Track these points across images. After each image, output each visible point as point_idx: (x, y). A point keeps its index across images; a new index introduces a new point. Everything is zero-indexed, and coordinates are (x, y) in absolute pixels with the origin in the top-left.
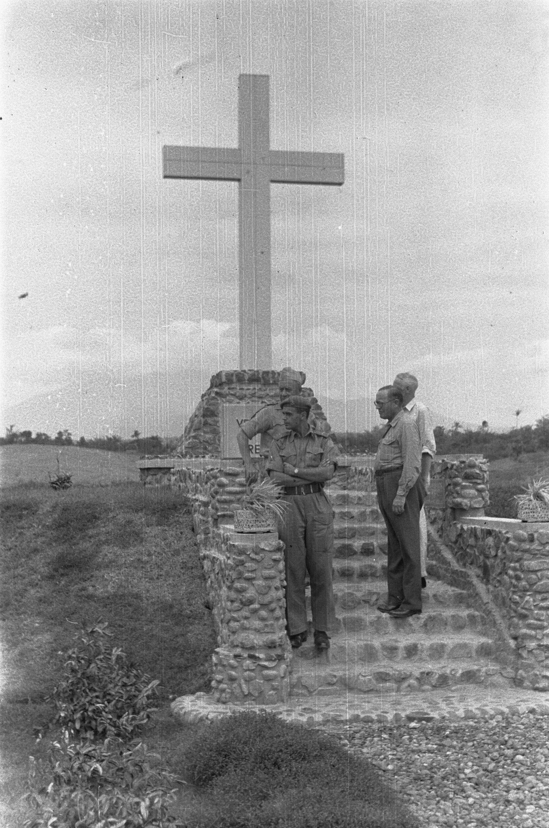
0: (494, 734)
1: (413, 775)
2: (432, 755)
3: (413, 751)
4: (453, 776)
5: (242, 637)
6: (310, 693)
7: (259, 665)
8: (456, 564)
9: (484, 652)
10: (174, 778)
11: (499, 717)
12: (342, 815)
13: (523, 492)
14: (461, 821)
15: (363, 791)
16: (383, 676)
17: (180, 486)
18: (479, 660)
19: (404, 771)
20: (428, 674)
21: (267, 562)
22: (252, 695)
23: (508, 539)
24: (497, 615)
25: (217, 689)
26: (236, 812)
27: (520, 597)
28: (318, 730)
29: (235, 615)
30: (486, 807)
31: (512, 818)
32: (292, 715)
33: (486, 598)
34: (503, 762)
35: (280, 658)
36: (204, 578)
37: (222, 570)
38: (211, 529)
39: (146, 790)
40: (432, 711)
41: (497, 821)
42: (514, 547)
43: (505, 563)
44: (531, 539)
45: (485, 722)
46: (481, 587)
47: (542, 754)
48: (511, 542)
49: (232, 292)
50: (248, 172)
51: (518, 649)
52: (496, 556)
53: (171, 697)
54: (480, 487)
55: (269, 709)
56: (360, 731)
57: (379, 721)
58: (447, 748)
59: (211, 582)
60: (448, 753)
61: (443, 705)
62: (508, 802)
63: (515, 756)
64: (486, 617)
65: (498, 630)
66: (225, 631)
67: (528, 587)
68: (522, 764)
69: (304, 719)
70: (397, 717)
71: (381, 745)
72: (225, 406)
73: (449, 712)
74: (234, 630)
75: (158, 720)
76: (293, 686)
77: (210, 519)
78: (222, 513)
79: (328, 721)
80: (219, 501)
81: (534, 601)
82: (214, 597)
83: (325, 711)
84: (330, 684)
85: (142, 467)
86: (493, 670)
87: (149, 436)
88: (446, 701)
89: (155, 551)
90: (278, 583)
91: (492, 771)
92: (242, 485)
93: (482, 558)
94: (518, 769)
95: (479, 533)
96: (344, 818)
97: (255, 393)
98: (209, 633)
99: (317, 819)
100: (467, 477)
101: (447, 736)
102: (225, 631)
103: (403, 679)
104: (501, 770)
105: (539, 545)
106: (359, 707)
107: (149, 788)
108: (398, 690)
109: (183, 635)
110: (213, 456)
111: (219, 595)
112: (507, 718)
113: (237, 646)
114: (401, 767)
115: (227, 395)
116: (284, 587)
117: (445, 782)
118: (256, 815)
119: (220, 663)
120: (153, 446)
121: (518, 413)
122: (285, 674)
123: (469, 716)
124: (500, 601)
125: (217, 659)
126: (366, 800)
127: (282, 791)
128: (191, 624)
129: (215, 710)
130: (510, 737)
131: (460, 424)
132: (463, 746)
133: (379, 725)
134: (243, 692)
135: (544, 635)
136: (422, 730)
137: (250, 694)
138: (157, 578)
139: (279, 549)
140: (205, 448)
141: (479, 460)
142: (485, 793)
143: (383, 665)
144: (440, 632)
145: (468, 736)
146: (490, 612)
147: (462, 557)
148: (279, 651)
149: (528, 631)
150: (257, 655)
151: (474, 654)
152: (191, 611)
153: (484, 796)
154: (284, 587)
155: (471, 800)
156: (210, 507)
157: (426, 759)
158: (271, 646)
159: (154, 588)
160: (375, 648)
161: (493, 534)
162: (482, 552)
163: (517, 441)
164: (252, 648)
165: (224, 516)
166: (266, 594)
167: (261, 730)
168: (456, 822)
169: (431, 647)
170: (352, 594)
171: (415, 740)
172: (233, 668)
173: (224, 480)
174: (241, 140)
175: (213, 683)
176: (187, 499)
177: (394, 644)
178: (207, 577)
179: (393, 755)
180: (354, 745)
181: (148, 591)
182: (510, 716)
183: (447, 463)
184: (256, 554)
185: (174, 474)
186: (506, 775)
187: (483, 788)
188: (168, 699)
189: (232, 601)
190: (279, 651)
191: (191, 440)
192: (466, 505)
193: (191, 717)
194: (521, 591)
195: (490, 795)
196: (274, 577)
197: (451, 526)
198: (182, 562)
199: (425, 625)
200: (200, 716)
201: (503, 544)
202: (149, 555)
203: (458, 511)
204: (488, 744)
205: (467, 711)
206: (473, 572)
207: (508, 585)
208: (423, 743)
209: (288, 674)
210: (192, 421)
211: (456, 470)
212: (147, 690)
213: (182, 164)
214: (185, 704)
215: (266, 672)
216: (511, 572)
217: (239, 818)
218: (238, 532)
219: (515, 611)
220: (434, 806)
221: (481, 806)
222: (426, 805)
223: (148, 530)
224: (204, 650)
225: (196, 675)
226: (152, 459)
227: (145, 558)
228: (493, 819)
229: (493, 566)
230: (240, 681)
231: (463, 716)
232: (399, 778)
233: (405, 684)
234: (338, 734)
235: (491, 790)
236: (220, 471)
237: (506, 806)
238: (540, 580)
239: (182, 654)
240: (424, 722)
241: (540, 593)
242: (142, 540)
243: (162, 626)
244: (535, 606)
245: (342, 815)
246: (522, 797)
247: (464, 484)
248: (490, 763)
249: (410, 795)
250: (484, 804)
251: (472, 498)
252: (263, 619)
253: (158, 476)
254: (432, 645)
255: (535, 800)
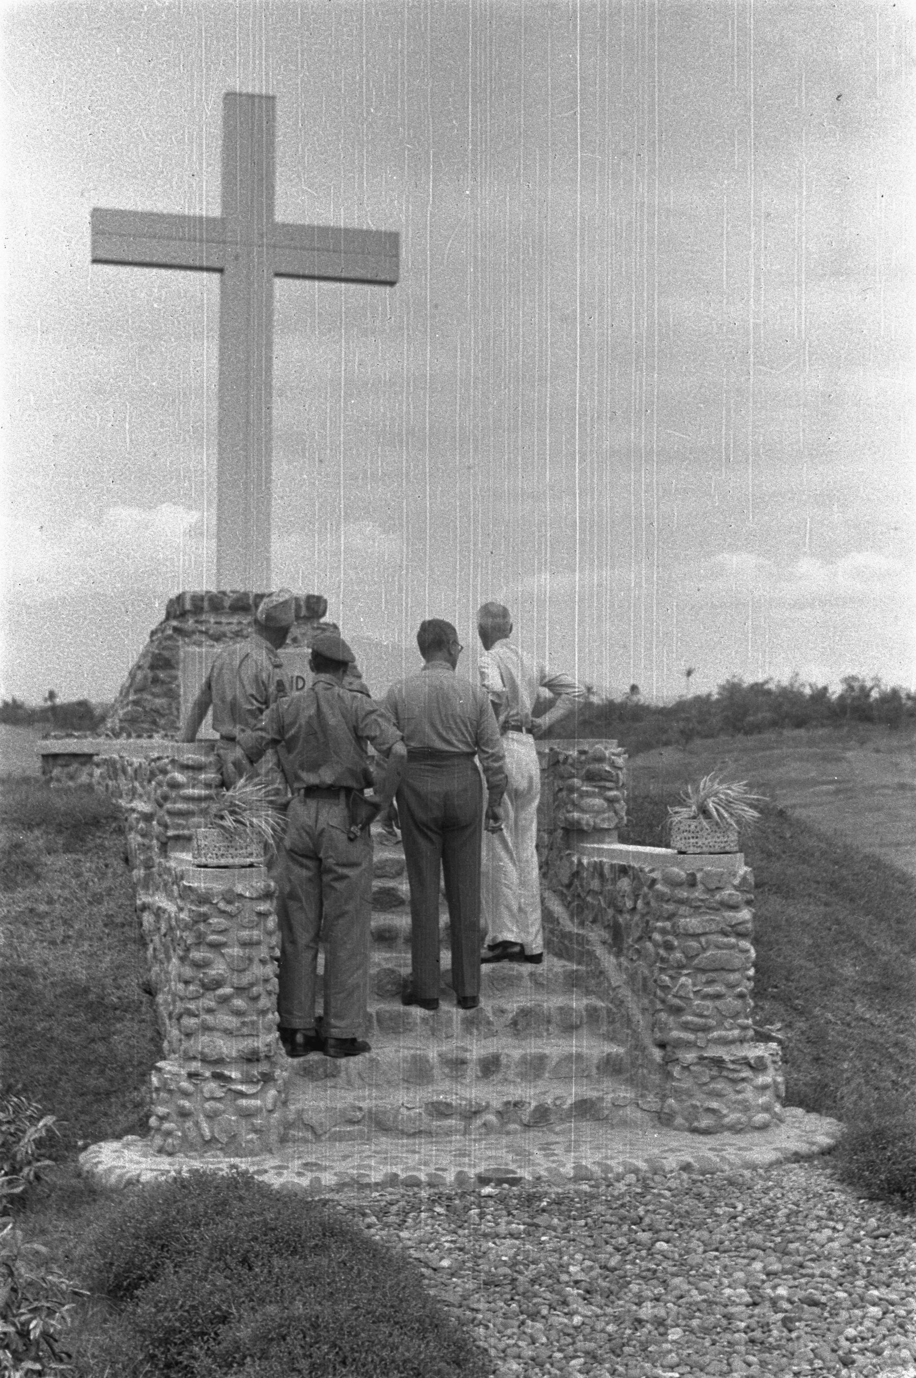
0: (623, 1206)
1: (483, 1277)
2: (517, 1242)
3: (485, 1235)
4: (550, 1277)
5: (201, 1043)
6: (318, 1137)
7: (230, 1090)
8: (569, 923)
9: (611, 1067)
10: (68, 1286)
11: (631, 1178)
12: (352, 1349)
13: (682, 803)
14: (559, 1355)
15: (392, 1306)
16: (442, 1108)
17: (107, 786)
18: (599, 1082)
19: (469, 1269)
20: (516, 1104)
21: (247, 917)
22: (218, 1141)
23: (654, 881)
24: (633, 1006)
25: (158, 1130)
26: (175, 1344)
27: (671, 977)
28: (328, 1200)
29: (192, 1006)
30: (603, 1331)
31: (645, 1350)
32: (281, 1173)
33: (617, 979)
34: (634, 1254)
35: (267, 1078)
36: (142, 941)
37: (171, 929)
38: (157, 861)
39: (19, 1308)
40: (520, 1167)
41: (619, 1356)
42: (663, 894)
43: (647, 922)
44: (692, 882)
45: (608, 1186)
46: (608, 961)
47: (699, 1240)
48: (658, 886)
49: (206, 460)
50: (237, 258)
51: (667, 1063)
52: (634, 909)
53: (80, 1143)
54: (612, 793)
55: (243, 1164)
56: (398, 1201)
57: (431, 1185)
58: (541, 1229)
59: (155, 949)
60: (543, 1238)
61: (538, 1156)
62: (639, 1322)
63: (653, 1244)
64: (615, 1010)
65: (634, 1031)
66: (175, 1033)
67: (684, 961)
68: (665, 1257)
69: (305, 1182)
70: (461, 1178)
71: (433, 1226)
72: (187, 650)
73: (548, 1169)
74: (189, 1031)
75: (55, 1183)
76: (288, 1125)
77: (155, 842)
78: (176, 832)
79: (344, 1185)
80: (170, 813)
81: (694, 985)
82: (158, 975)
83: (340, 1166)
84: (351, 1122)
85: (45, 752)
86: (624, 1097)
87: (74, 699)
88: (544, 1149)
89: (60, 896)
90: (264, 952)
91: (615, 1269)
92: (208, 786)
93: (611, 912)
94: (658, 1265)
95: (606, 870)
96: (356, 1355)
97: (241, 630)
98: (149, 1034)
99: (311, 1356)
100: (590, 777)
101: (544, 1210)
102: (175, 1033)
103: (475, 1113)
104: (628, 1267)
105: (704, 892)
106: (395, 1161)
107: (24, 1304)
108: (466, 1132)
109: (104, 1038)
110: (166, 735)
111: (167, 973)
112: (644, 1179)
113: (194, 1058)
114: (464, 1262)
115: (193, 632)
116: (277, 959)
117: (537, 1287)
118: (208, 1349)
119: (164, 1086)
120: (78, 717)
121: (689, 673)
122: (275, 1105)
123: (582, 1175)
124: (639, 985)
125: (159, 1079)
126: (396, 1323)
127: (253, 1308)
128: (120, 1019)
129: (154, 1167)
130: (647, 1211)
131: (595, 690)
132: (569, 1226)
133: (432, 1191)
134: (202, 1136)
135: (709, 1041)
136: (502, 1199)
137: (213, 1140)
138: (63, 942)
139: (267, 895)
140: (154, 722)
141: (611, 749)
142: (601, 1308)
143: (444, 1091)
144: (539, 1036)
145: (577, 1209)
146: (622, 1002)
147: (578, 910)
148: (264, 1067)
149: (684, 1035)
150: (227, 1073)
151: (594, 1071)
152: (119, 998)
153: (599, 1311)
154: (277, 959)
155: (577, 1320)
156: (155, 823)
157: (505, 1250)
158: (252, 1058)
159: (56, 959)
160: (428, 1061)
161: (631, 873)
162: (612, 903)
163: (687, 720)
164: (220, 1061)
165: (177, 838)
166: (244, 970)
167: (225, 1203)
168: (550, 1357)
169: (524, 1060)
170: (393, 971)
171: (489, 1217)
172: (186, 1094)
173: (180, 777)
174: (225, 205)
175: (153, 1121)
176: (118, 808)
177: (462, 1055)
178: (148, 939)
179: (451, 1242)
180: (387, 1225)
181: (46, 963)
182: (649, 1175)
183: (557, 754)
184: (229, 902)
185: (98, 765)
186: (639, 1276)
187: (598, 1298)
188: (75, 1146)
189: (187, 983)
190: (264, 1067)
191: (129, 708)
192: (588, 824)
193: (113, 1179)
194: (672, 968)
195: (609, 1310)
196: (258, 943)
197: (561, 858)
198: (107, 916)
199: (515, 1023)
200: (128, 1176)
201: (646, 889)
202: (50, 902)
203: (574, 833)
204: (611, 1223)
205: (578, 1167)
206: (596, 935)
207: (653, 959)
208: (503, 1221)
209: (279, 1104)
210: (132, 675)
211: (572, 765)
212: (33, 1133)
213: (123, 240)
214: (103, 1157)
215: (244, 1102)
216: (657, 936)
217: (179, 1354)
218: (199, 866)
219: (663, 1001)
220: (515, 1330)
221: (593, 1329)
222: (501, 1328)
223: (49, 860)
224: (141, 1063)
225: (124, 1106)
226: (61, 738)
227: (43, 908)
228: (613, 1352)
229: (628, 927)
230: (198, 1116)
231: (572, 1175)
232: (459, 1281)
233: (479, 1122)
234: (361, 1207)
235: (613, 1302)
236: (173, 761)
237: (636, 1329)
238: (704, 950)
239: (102, 1072)
240: (506, 1186)
241: (704, 971)
242: (38, 877)
243: (70, 1024)
244: (695, 993)
245: (352, 1349)
246: (662, 1313)
247: (584, 788)
248: (611, 1255)
249: (477, 1311)
250: (599, 1326)
251: (598, 812)
252: (238, 1013)
253: (72, 769)
254: (524, 1058)
255: (685, 1318)
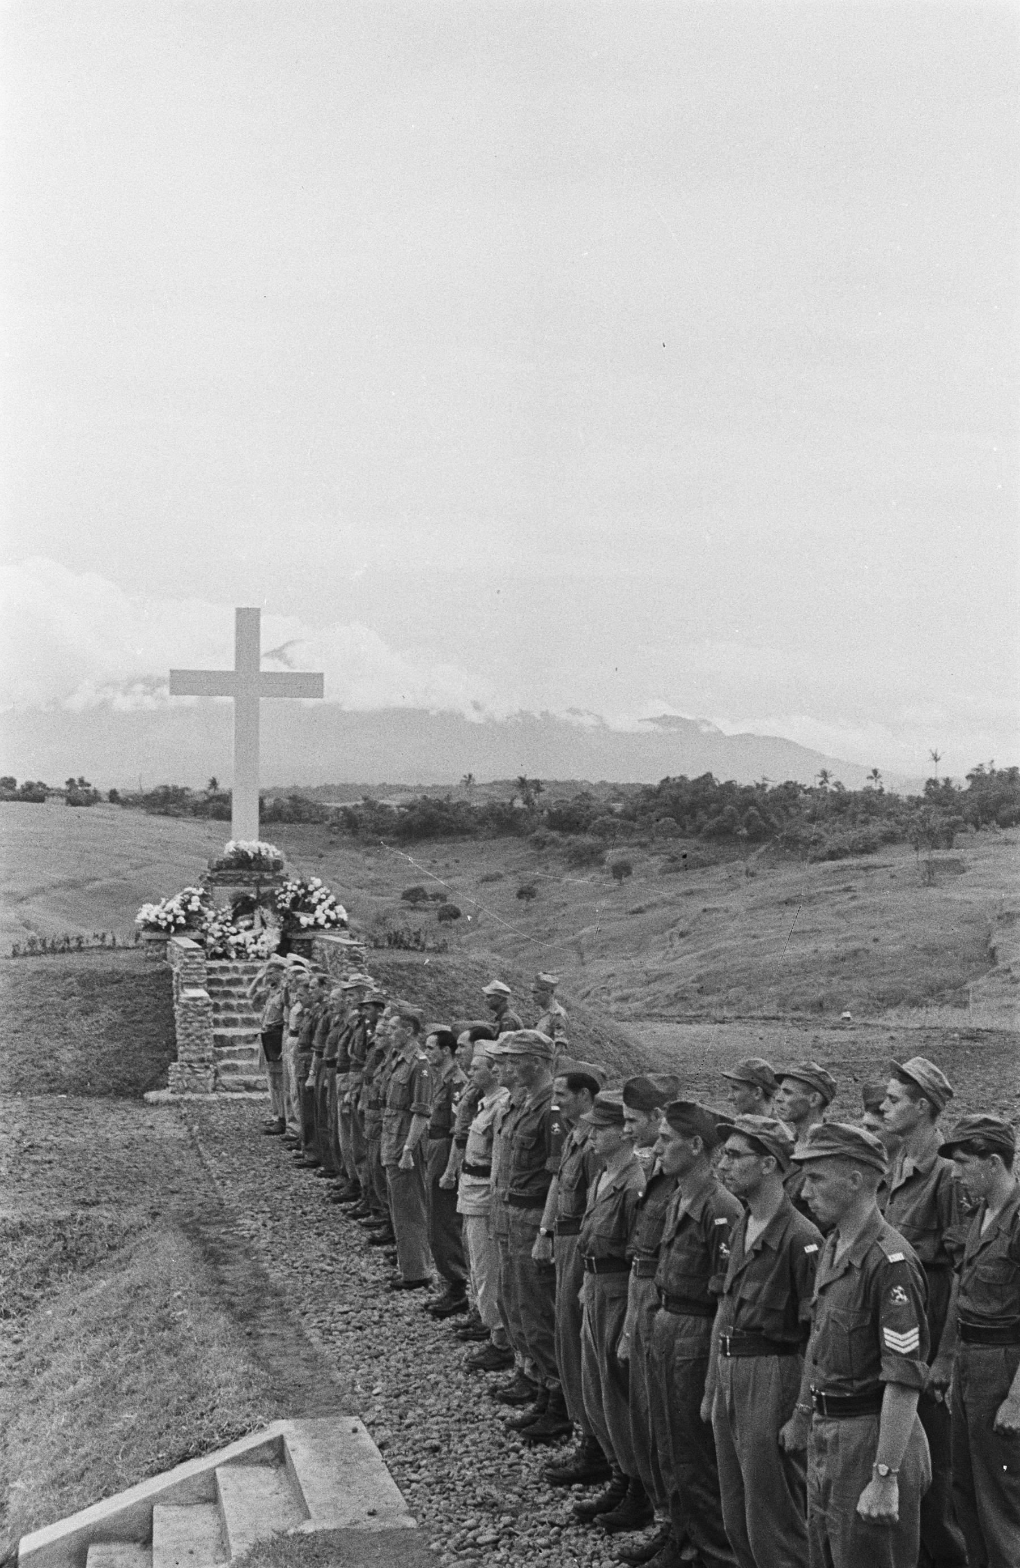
164: (191, 1061)
252: (197, 1045)
